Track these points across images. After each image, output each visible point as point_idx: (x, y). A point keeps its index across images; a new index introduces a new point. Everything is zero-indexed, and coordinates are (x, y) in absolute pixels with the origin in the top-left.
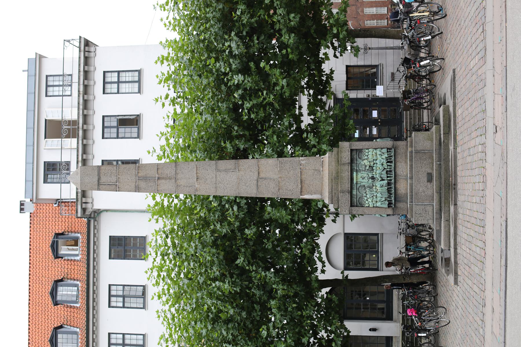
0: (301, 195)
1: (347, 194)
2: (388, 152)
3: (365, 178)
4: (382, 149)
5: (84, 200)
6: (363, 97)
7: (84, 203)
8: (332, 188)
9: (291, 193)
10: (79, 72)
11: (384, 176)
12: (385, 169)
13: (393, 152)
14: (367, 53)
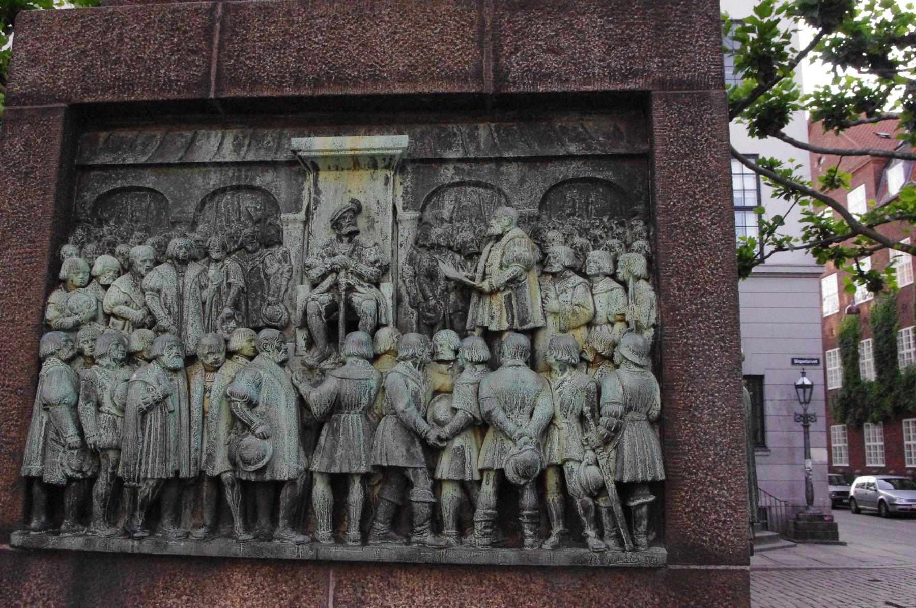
2: (626, 490)
3: (344, 247)
4: (660, 423)
12: (433, 452)
13: (629, 558)
14: (796, 421)
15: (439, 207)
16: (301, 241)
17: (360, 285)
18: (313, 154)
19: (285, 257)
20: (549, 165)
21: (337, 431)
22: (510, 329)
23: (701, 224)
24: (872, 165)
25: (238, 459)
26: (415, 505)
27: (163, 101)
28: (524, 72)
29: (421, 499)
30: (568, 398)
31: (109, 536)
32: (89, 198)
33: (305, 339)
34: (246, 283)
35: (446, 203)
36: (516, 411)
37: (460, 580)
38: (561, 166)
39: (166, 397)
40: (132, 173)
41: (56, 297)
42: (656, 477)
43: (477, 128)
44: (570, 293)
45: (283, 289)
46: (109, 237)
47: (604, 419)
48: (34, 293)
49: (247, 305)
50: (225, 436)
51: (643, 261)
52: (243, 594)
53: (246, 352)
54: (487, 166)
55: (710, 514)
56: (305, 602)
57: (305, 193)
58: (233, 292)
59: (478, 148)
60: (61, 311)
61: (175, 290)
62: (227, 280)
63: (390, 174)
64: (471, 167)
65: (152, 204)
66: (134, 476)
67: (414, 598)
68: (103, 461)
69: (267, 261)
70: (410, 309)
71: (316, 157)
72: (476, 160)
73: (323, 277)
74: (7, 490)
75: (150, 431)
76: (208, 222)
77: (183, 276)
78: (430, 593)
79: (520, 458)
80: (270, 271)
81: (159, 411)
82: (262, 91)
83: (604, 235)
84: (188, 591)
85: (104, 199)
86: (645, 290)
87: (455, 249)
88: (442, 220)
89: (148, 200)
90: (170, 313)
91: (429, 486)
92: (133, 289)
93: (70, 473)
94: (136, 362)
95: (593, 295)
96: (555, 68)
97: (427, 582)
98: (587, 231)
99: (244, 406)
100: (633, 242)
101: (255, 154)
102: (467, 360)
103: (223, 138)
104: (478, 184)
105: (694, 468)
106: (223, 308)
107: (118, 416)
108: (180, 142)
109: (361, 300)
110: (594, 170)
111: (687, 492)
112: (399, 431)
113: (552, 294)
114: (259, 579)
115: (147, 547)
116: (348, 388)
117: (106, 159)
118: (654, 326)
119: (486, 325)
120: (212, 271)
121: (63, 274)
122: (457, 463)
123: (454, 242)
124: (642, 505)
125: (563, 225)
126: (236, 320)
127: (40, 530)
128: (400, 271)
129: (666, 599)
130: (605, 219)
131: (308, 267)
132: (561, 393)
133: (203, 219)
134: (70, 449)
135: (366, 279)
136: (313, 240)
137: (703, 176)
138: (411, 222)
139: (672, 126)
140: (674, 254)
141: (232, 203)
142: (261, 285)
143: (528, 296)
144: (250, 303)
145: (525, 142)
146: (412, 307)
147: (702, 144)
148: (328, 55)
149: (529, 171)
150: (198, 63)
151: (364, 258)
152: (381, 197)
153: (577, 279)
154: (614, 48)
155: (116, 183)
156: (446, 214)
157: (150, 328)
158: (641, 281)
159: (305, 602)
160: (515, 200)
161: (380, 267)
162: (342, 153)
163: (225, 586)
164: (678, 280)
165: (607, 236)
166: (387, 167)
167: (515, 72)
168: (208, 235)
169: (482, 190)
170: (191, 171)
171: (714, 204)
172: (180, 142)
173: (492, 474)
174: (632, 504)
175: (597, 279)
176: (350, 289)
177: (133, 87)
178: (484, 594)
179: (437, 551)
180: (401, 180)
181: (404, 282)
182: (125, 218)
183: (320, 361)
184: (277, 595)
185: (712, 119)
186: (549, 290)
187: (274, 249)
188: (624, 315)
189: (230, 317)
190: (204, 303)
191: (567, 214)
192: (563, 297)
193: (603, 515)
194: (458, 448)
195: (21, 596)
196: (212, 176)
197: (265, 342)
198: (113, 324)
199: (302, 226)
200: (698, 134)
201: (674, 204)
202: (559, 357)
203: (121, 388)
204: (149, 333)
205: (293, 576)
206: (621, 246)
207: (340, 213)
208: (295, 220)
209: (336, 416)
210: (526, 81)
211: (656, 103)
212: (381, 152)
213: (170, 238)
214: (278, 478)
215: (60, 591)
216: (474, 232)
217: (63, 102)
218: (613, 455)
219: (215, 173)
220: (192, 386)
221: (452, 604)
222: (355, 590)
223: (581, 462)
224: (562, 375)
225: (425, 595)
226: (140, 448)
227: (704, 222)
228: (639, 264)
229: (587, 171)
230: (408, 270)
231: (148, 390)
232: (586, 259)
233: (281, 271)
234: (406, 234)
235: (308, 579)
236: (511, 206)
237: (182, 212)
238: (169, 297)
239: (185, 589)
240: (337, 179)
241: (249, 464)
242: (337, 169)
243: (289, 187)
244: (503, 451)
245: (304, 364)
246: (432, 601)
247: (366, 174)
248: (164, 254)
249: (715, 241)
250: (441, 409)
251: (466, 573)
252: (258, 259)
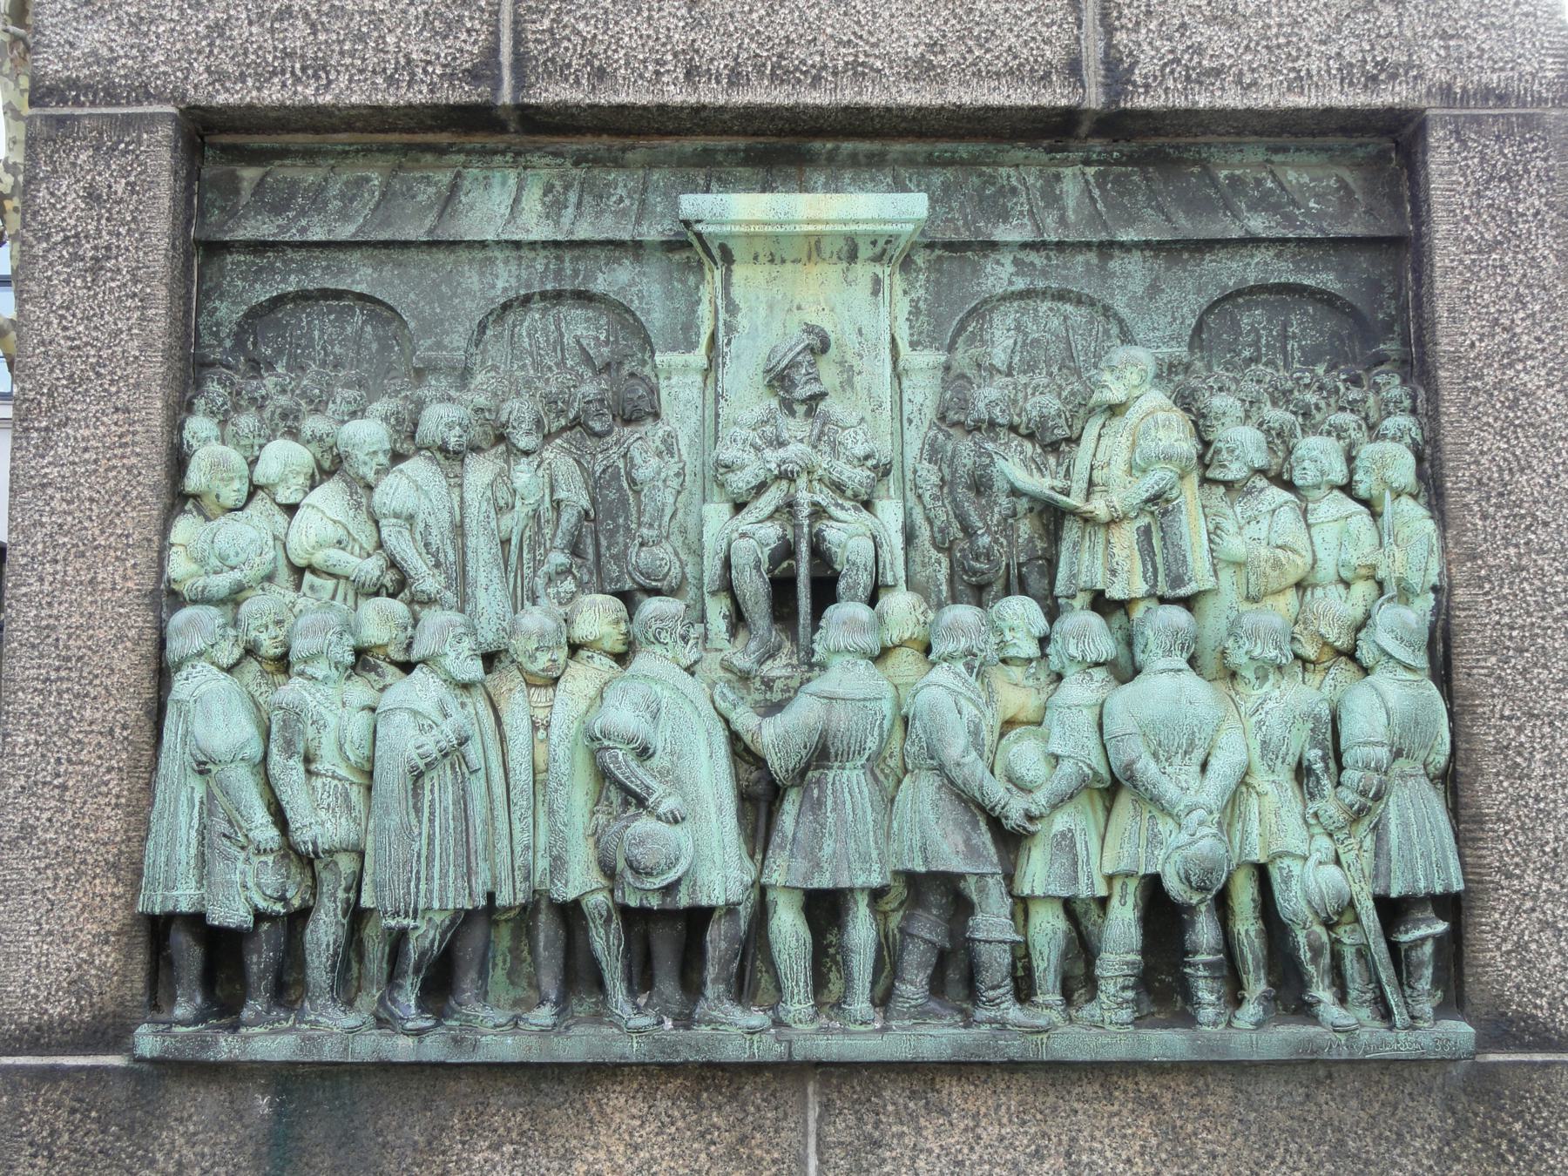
1: (469, 46)
2: (1393, 911)
3: (796, 427)
4: (1451, 781)
13: (1401, 1043)
15: (983, 342)
16: (699, 411)
17: (837, 505)
18: (726, 229)
19: (669, 447)
20: (1208, 257)
21: (819, 804)
22: (1150, 596)
23: (1525, 385)
25: (621, 865)
26: (982, 947)
27: (397, 108)
28: (1165, 65)
29: (996, 935)
30: (1278, 733)
31: (352, 1031)
32: (228, 312)
33: (725, 617)
34: (594, 501)
35: (998, 333)
36: (1177, 760)
37: (1069, 1092)
38: (1232, 259)
39: (463, 741)
40: (321, 259)
41: (185, 529)
42: (1450, 885)
43: (1058, 178)
44: (1264, 525)
45: (668, 512)
46: (283, 400)
47: (1350, 775)
48: (138, 519)
49: (597, 545)
50: (586, 819)
51: (1410, 459)
52: (631, 1135)
53: (608, 645)
54: (1080, 258)
55: (1549, 955)
56: (759, 1146)
57: (704, 310)
58: (568, 518)
59: (1062, 220)
60: (201, 561)
61: (446, 515)
62: (552, 495)
63: (883, 271)
64: (1048, 258)
65: (368, 328)
66: (407, 905)
67: (979, 1131)
68: (325, 875)
69: (635, 453)
70: (934, 553)
71: (732, 236)
72: (1060, 246)
73: (761, 488)
74: (107, 942)
75: (432, 814)
76: (495, 368)
77: (461, 486)
78: (1010, 1121)
79: (1191, 851)
80: (641, 474)
81: (449, 772)
82: (616, 92)
83: (1322, 404)
84: (514, 1135)
85: (260, 315)
86: (1413, 518)
87: (1023, 430)
88: (993, 370)
89: (359, 318)
90: (437, 565)
91: (1007, 911)
92: (352, 513)
93: (262, 904)
94: (374, 668)
95: (1308, 526)
96: (1230, 56)
97: (1004, 1099)
98: (1287, 393)
99: (630, 758)
100: (1382, 419)
101: (592, 223)
102: (1072, 659)
103: (520, 189)
104: (1061, 296)
105: (1517, 865)
106: (547, 552)
107: (352, 783)
108: (426, 194)
109: (844, 536)
110: (1298, 269)
111: (1503, 914)
112: (948, 805)
113: (1229, 525)
114: (662, 1105)
115: (434, 1049)
116: (842, 718)
117: (251, 229)
118: (1435, 589)
119: (1099, 586)
120: (523, 474)
121: (195, 480)
122: (1062, 865)
123: (1019, 415)
124: (1423, 939)
125: (1237, 381)
126: (574, 577)
127: (195, 1023)
128: (909, 476)
129: (1467, 1119)
130: (1320, 370)
131: (726, 466)
132: (1260, 723)
133: (483, 362)
134: (259, 852)
135: (849, 493)
136: (727, 410)
137: (1529, 286)
138: (931, 372)
139: (1468, 185)
140: (1473, 446)
141: (545, 329)
142: (624, 502)
143: (1184, 530)
144: (604, 542)
145: (1160, 209)
146: (939, 549)
147: (1527, 222)
148: (755, 16)
149: (1168, 269)
150: (469, 25)
151: (842, 449)
152: (865, 321)
153: (1277, 495)
154: (1348, 16)
155: (284, 281)
156: (999, 357)
157: (393, 596)
158: (1404, 499)
159: (759, 1146)
160: (1140, 330)
161: (875, 467)
162: (789, 228)
163: (591, 1121)
164: (1481, 498)
165: (1328, 405)
166: (878, 259)
167: (1146, 66)
168: (499, 398)
169: (1069, 308)
170: (452, 257)
171: (1550, 344)
172: (426, 194)
173: (1133, 885)
174: (1404, 938)
175: (1316, 494)
176: (818, 512)
177: (327, 73)
178: (1116, 1119)
179: (1030, 1037)
180: (904, 286)
181: (920, 497)
182: (309, 357)
183: (761, 662)
184: (703, 1135)
185: (1547, 170)
186: (1224, 516)
187: (648, 425)
188: (1374, 567)
189: (566, 572)
190: (505, 542)
191: (1245, 360)
192: (1252, 530)
193: (1347, 962)
194: (1063, 834)
195: (153, 1162)
196: (501, 268)
197: (659, 624)
198: (312, 587)
199: (699, 378)
200: (1518, 201)
201: (1473, 345)
202: (1255, 654)
203: (358, 725)
204: (398, 607)
205: (733, 1098)
206: (1360, 427)
207: (790, 355)
208: (686, 366)
209: (817, 774)
210: (1170, 84)
211: (1436, 136)
212: (870, 227)
213: (420, 405)
214: (704, 902)
215: (241, 1145)
216: (1059, 395)
217: (168, 101)
218: (1368, 843)
219: (506, 261)
220: (506, 718)
221: (1055, 1140)
222: (860, 1119)
223: (1305, 859)
224: (1261, 687)
225: (1001, 1125)
226: (416, 847)
227: (1532, 382)
228: (1403, 469)
229: (1284, 271)
230: (930, 475)
231: (421, 729)
232: (1290, 452)
233: (663, 475)
234: (919, 399)
235: (764, 1100)
236: (1133, 342)
237: (439, 345)
238: (434, 532)
239: (509, 1130)
240: (771, 281)
241: (649, 874)
242: (772, 261)
243: (669, 295)
244: (1154, 840)
245: (727, 667)
246: (1014, 1135)
247: (832, 272)
248: (412, 436)
249: (1553, 419)
250: (1025, 754)
251: (1080, 1079)
252: (615, 449)
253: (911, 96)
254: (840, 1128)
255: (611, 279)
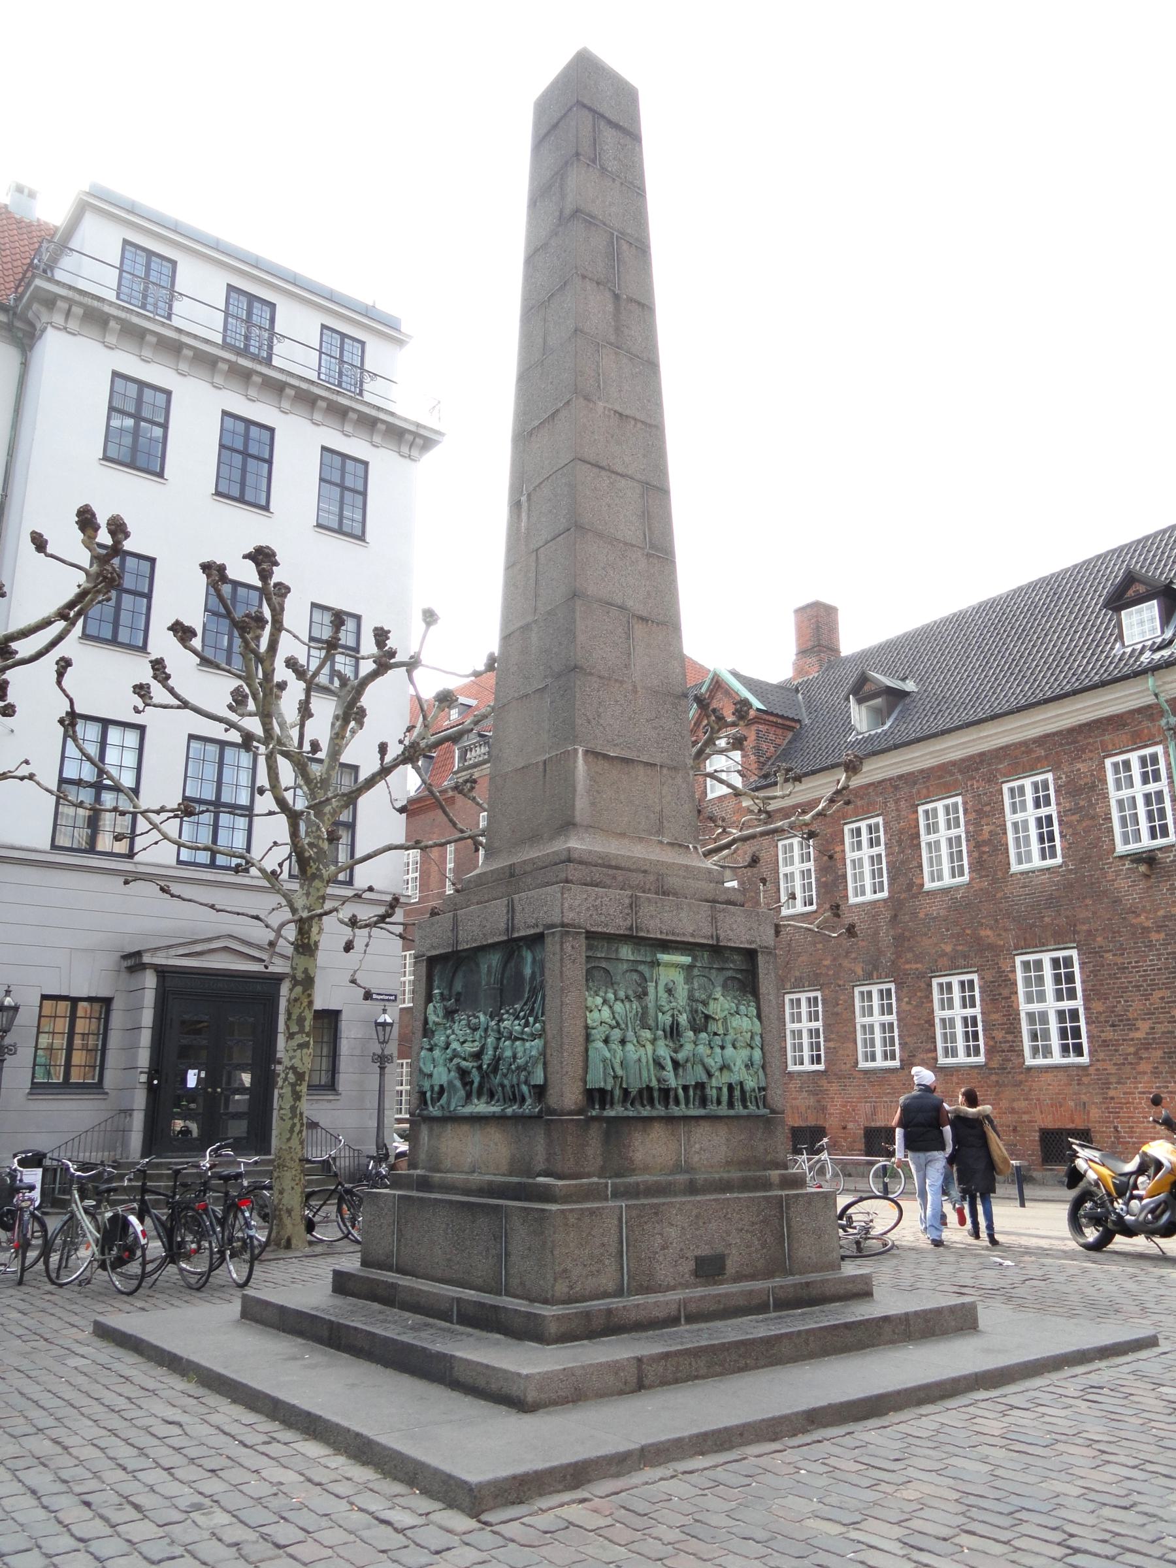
0: (586, 752)
1: (629, 923)
4: (763, 1067)
5: (78, 311)
6: (278, 1049)
7: (69, 310)
8: (617, 868)
9: (591, 717)
10: (379, 409)
11: (694, 1075)
14: (373, 1062)
24: (81, 577)
108: (614, 949)
253: (691, 940)
254: (686, 1129)
255: (641, 968)
